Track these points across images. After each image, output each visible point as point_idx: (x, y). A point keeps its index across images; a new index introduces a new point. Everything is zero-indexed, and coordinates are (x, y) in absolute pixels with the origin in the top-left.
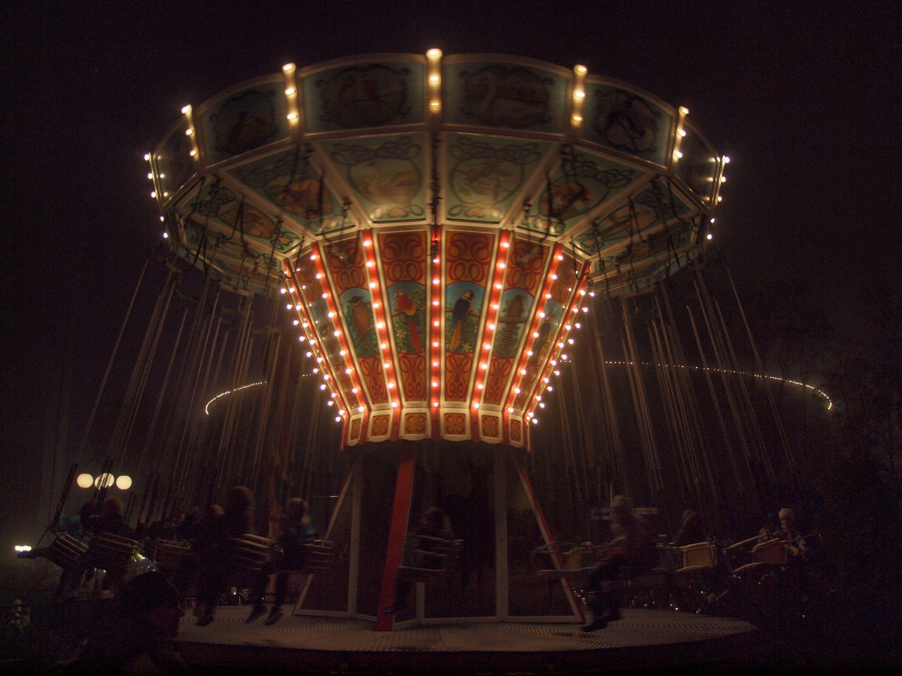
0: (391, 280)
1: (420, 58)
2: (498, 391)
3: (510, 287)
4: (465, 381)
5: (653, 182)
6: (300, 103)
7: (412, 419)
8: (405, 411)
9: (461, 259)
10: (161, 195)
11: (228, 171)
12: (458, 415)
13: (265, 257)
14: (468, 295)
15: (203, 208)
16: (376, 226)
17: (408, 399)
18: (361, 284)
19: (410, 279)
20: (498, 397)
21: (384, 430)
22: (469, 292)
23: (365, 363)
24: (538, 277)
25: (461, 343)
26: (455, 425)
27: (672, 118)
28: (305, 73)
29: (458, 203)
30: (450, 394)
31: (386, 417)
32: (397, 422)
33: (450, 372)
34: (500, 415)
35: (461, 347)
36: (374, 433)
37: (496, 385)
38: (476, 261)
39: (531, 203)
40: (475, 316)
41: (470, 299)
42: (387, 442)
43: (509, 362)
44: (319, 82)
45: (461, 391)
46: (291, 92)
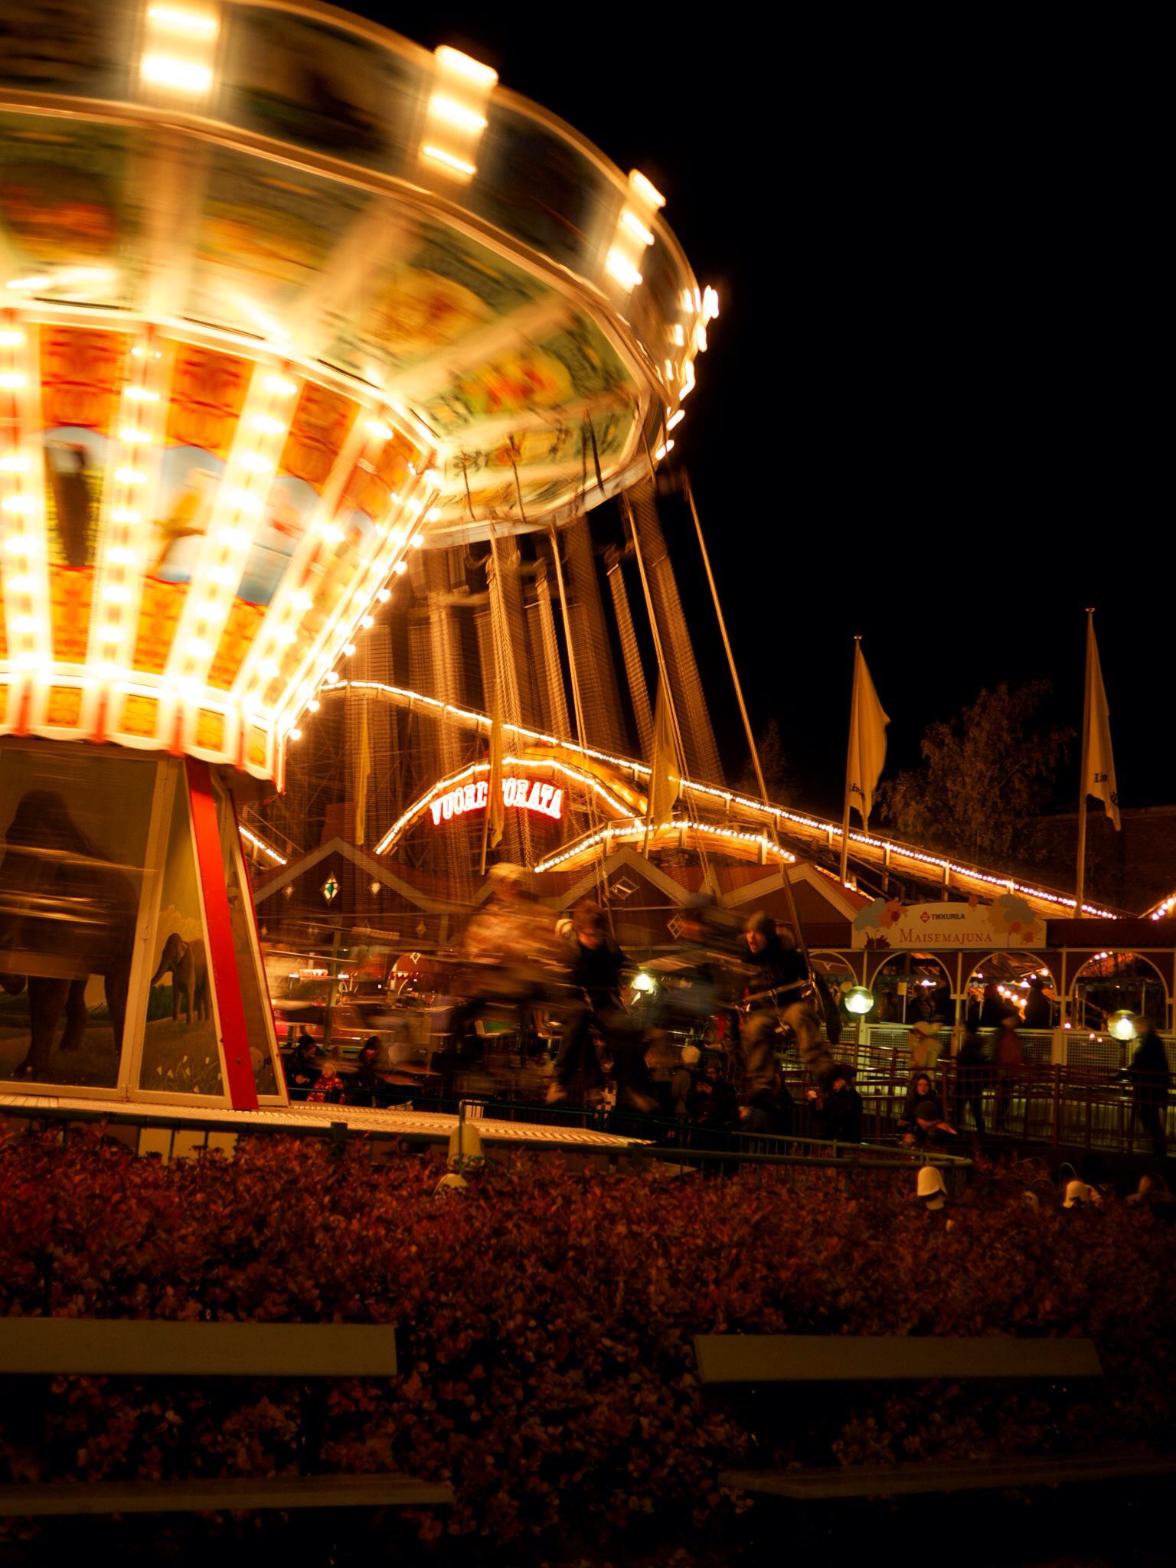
42: (85, 743)
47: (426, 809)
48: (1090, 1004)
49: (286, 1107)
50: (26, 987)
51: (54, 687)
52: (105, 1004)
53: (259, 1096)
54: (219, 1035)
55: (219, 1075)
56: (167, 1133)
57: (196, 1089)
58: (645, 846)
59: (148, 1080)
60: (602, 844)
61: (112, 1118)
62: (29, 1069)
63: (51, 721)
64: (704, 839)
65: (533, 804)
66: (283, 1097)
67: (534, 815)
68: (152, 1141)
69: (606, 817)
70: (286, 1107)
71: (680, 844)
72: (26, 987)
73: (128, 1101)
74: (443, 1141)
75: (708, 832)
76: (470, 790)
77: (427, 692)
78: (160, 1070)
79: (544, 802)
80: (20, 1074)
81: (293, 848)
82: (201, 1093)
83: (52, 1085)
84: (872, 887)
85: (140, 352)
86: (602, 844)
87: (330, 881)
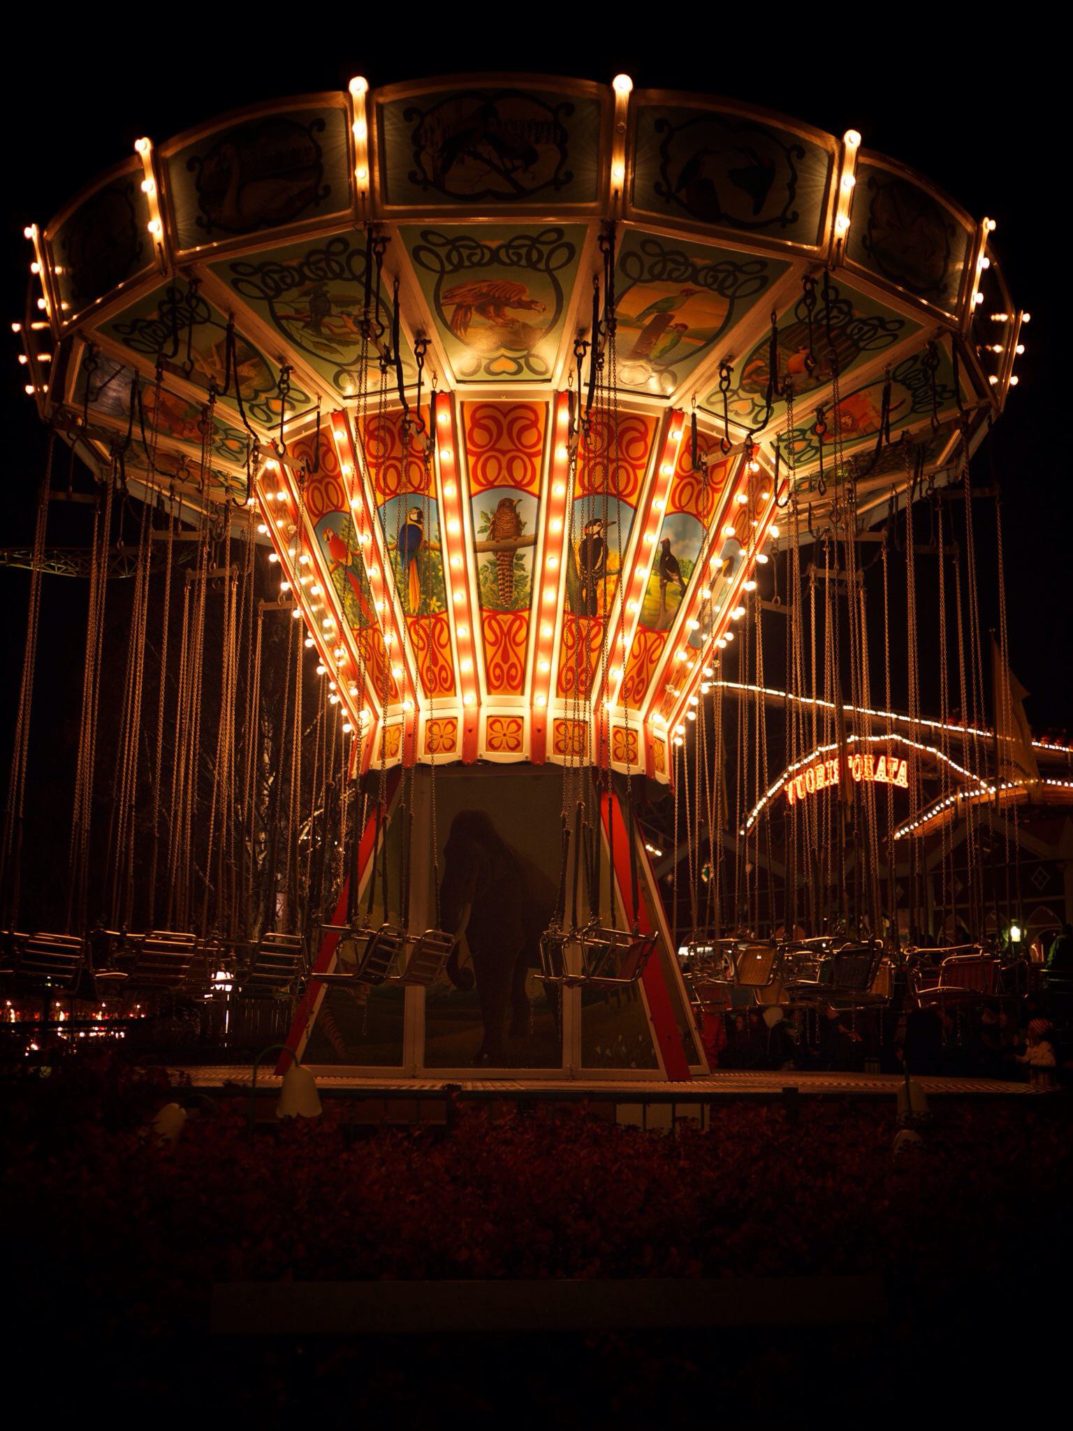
0: (478, 482)
1: (591, 86)
2: (444, 674)
3: (675, 510)
4: (446, 661)
5: (931, 344)
6: (376, 154)
7: (498, 724)
8: (485, 712)
9: (389, 458)
10: (56, 306)
11: (211, 266)
12: (511, 719)
13: (227, 434)
14: (414, 517)
15: (136, 335)
16: (462, 387)
17: (493, 691)
18: (422, 489)
19: (512, 483)
20: (641, 695)
21: (448, 744)
22: (415, 510)
23: (642, 636)
24: (717, 496)
25: (425, 599)
26: (505, 735)
27: (969, 236)
28: (388, 96)
29: (337, 369)
30: (496, 683)
31: (452, 721)
32: (471, 731)
33: (492, 644)
34: (639, 727)
35: (426, 605)
36: (430, 749)
37: (638, 676)
38: (626, 461)
39: (732, 365)
40: (433, 549)
41: (419, 521)
42: (458, 764)
43: (661, 637)
44: (409, 112)
45: (445, 680)
46: (360, 130)
47: (780, 792)
48: (300, 1052)
49: (708, 1075)
50: (475, 984)
51: (555, 719)
52: (544, 994)
53: (690, 1067)
54: (649, 1015)
55: (653, 1051)
56: (638, 1108)
57: (633, 1065)
58: (997, 805)
59: (589, 1059)
60: (953, 808)
61: (591, 1095)
62: (486, 1056)
63: (491, 746)
64: (1053, 792)
65: (881, 777)
66: (704, 1066)
67: (881, 786)
68: (627, 1115)
69: (958, 783)
70: (708, 1075)
71: (1029, 800)
72: (475, 984)
73: (574, 1079)
74: (891, 1098)
75: (1056, 785)
76: (820, 769)
77: (628, 690)
78: (598, 1049)
79: (891, 776)
80: (478, 1062)
81: (665, 839)
82: (638, 1067)
83: (507, 1070)
84: (152, 899)
85: (339, 436)
86: (953, 808)
87: (706, 866)
